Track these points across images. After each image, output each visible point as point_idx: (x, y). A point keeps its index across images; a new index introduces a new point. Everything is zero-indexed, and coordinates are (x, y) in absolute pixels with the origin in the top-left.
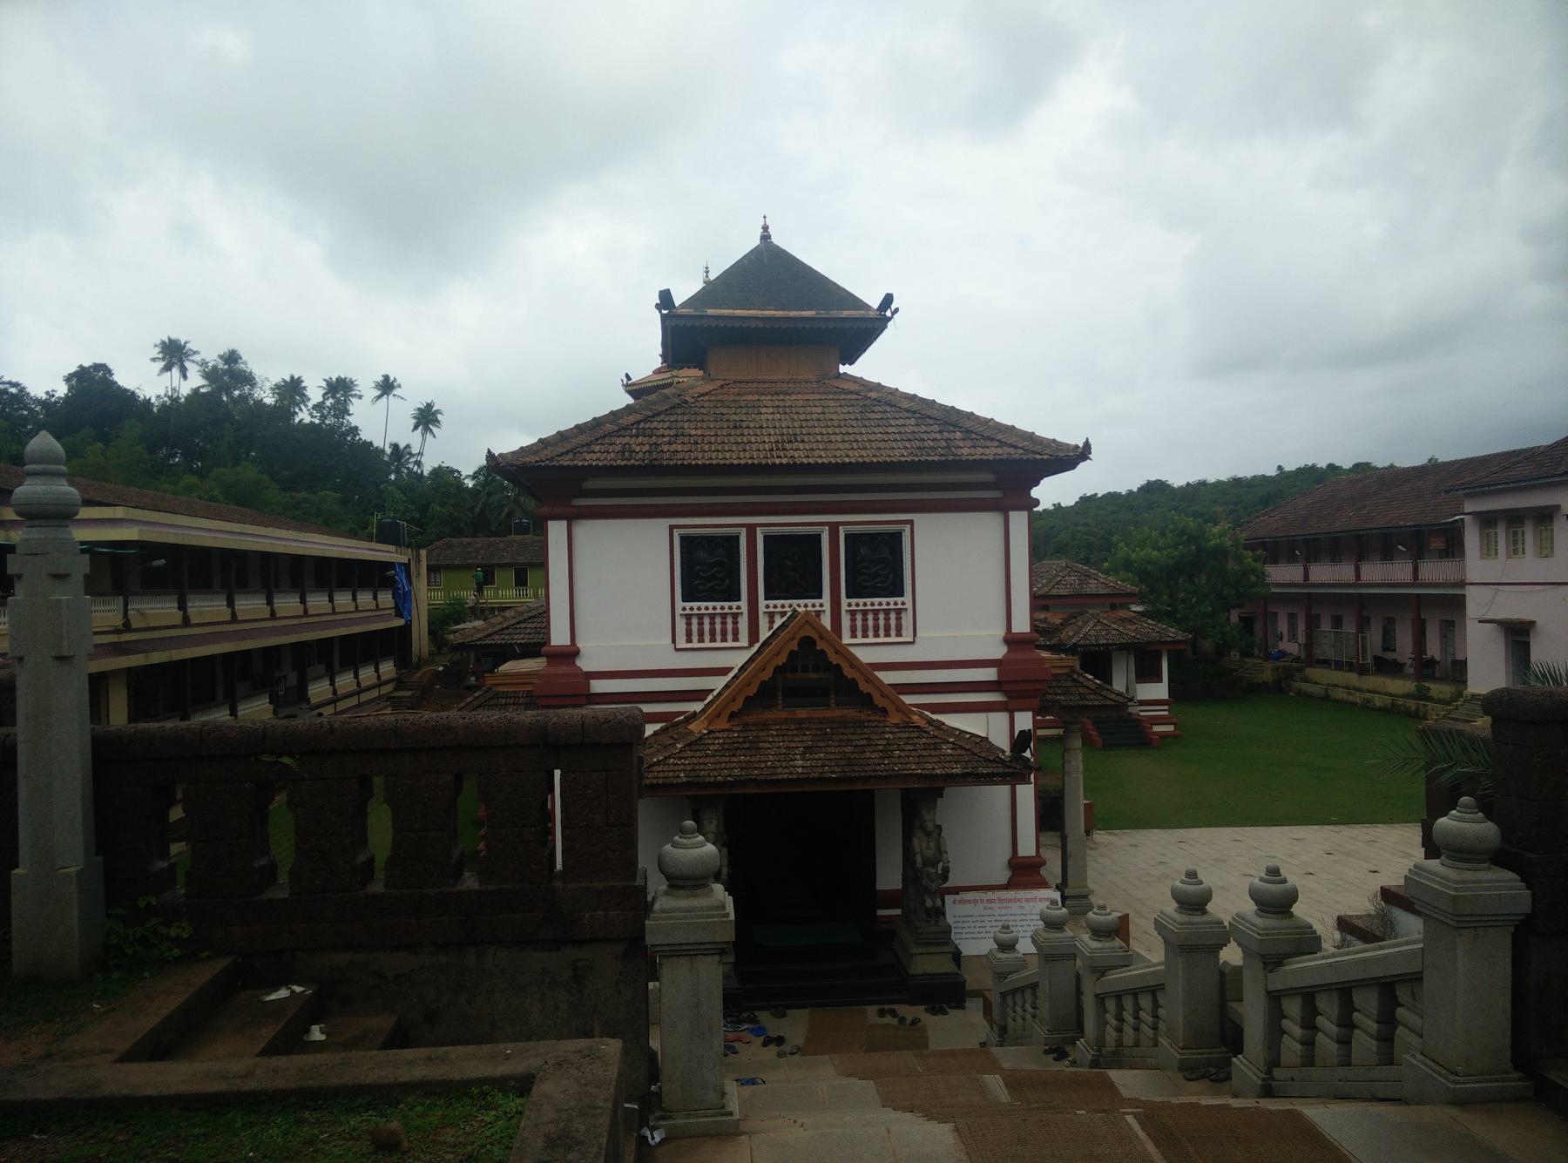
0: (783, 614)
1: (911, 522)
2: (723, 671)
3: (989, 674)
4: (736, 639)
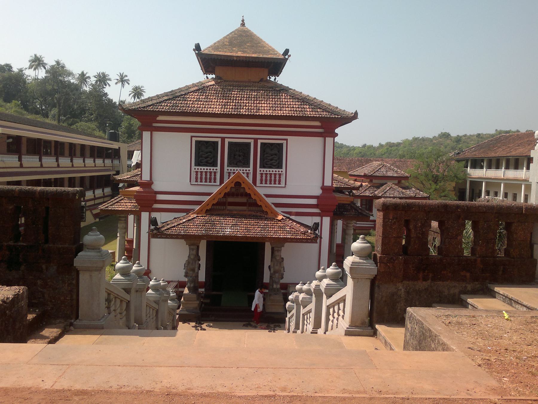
0: (234, 173)
1: (287, 140)
2: (209, 194)
3: (314, 202)
4: (215, 182)
